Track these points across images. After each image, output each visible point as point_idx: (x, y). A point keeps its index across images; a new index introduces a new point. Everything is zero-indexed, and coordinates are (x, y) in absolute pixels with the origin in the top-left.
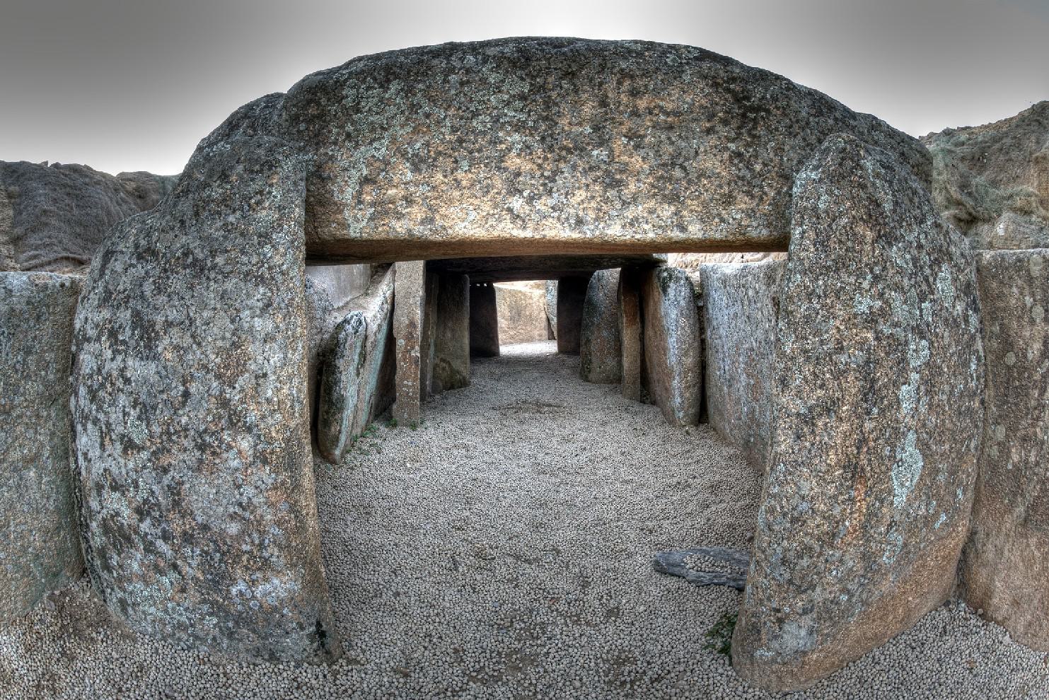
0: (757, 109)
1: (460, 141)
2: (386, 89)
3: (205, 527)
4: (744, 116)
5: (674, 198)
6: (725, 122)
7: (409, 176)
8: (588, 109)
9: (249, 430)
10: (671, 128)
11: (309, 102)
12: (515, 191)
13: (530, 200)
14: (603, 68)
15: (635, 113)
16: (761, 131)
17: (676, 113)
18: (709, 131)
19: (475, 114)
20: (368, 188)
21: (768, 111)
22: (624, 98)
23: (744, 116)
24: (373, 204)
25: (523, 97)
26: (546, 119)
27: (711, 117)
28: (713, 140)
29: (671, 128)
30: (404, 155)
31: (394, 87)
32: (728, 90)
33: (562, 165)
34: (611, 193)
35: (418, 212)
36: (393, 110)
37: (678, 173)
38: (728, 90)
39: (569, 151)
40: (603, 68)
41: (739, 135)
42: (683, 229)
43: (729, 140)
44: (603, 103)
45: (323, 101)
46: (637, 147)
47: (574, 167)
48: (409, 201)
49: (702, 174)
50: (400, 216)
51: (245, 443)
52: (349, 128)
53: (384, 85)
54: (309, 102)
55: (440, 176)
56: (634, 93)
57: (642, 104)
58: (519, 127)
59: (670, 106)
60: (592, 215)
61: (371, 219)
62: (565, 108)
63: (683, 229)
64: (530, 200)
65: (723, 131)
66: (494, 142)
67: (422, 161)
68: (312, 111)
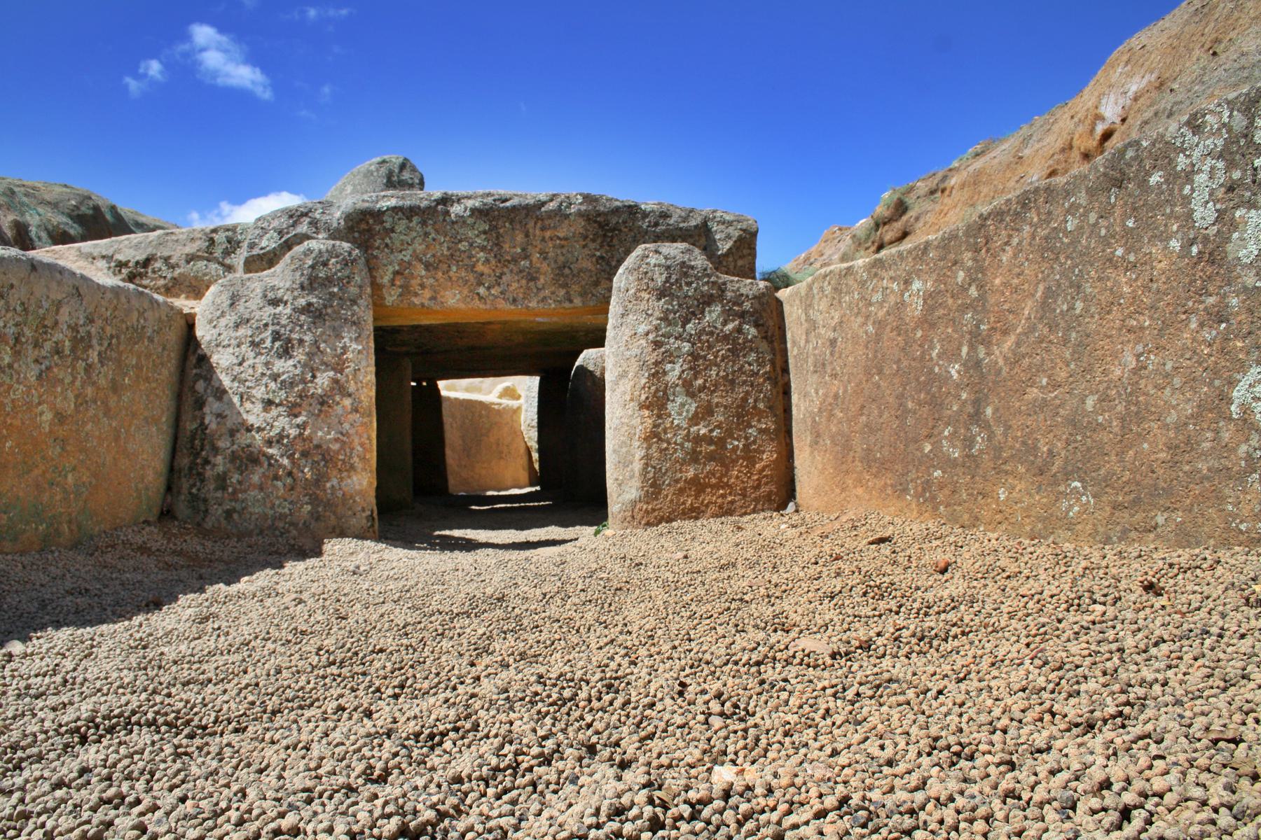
0: (613, 230)
1: (452, 255)
2: (411, 221)
3: (318, 447)
4: (605, 235)
5: (565, 286)
6: (593, 241)
7: (423, 273)
8: (520, 238)
9: (350, 395)
10: (563, 247)
11: (361, 220)
12: (480, 284)
13: (489, 288)
14: (527, 215)
15: (543, 240)
16: (615, 242)
17: (566, 239)
18: (584, 247)
19: (460, 241)
20: (398, 277)
21: (620, 231)
22: (538, 232)
23: (605, 235)
24: (401, 287)
25: (485, 232)
26: (497, 245)
27: (586, 238)
28: (586, 251)
29: (563, 247)
30: (421, 260)
31: (416, 219)
32: (596, 222)
33: (505, 270)
34: (532, 284)
35: (427, 294)
36: (414, 234)
37: (567, 271)
38: (596, 222)
39: (509, 262)
40: (527, 215)
41: (602, 246)
42: (571, 301)
43: (596, 250)
44: (527, 236)
45: (371, 221)
46: (545, 258)
47: (511, 271)
48: (422, 286)
49: (581, 270)
50: (416, 295)
51: (347, 402)
52: (387, 240)
53: (409, 219)
54: (361, 220)
55: (440, 274)
56: (543, 229)
57: (548, 234)
58: (483, 249)
59: (561, 235)
60: (521, 296)
61: (401, 295)
62: (507, 238)
63: (571, 301)
64: (489, 288)
65: (592, 246)
66: (470, 257)
67: (431, 265)
68: (363, 226)
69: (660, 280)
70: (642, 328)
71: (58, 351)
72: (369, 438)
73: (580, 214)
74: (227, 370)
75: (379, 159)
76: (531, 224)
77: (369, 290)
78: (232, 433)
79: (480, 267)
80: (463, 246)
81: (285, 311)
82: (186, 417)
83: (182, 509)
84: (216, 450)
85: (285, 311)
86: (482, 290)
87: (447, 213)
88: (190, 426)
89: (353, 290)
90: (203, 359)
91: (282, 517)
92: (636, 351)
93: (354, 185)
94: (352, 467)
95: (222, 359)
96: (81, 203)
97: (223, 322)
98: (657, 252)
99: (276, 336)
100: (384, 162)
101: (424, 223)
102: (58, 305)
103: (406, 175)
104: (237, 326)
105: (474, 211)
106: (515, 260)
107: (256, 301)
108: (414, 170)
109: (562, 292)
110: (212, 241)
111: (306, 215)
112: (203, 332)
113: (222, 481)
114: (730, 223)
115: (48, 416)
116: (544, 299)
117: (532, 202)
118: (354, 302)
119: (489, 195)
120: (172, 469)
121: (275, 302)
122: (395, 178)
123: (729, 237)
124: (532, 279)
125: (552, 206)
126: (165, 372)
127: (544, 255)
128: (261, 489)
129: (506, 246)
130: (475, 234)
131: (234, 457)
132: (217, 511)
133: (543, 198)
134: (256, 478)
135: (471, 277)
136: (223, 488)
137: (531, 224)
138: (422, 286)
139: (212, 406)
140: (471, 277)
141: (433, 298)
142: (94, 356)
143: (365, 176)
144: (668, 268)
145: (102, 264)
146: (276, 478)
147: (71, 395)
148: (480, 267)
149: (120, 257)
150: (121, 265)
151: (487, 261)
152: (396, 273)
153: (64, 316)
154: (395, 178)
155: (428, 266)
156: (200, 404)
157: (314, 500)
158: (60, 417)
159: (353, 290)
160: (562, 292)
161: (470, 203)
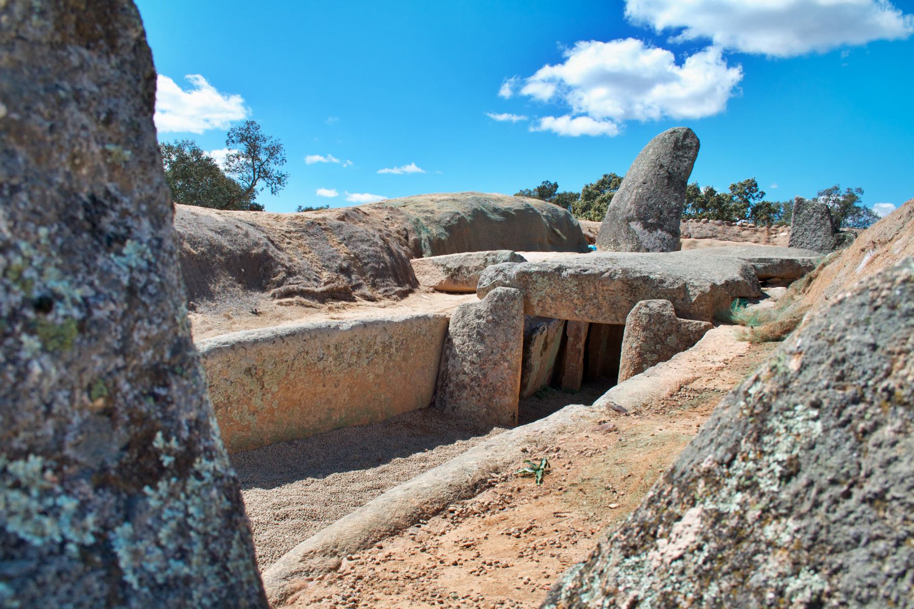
5: (614, 313)
8: (592, 289)
35: (553, 311)
51: (506, 364)
56: (603, 286)
57: (605, 288)
58: (576, 293)
69: (645, 321)
70: (634, 345)
71: (376, 352)
72: (515, 381)
73: (619, 279)
74: (458, 346)
75: (671, 130)
76: (597, 283)
77: (522, 312)
78: (457, 374)
79: (575, 301)
80: (567, 291)
81: (483, 321)
82: (442, 364)
83: (437, 404)
84: (451, 381)
85: (483, 321)
86: (577, 312)
87: (560, 275)
88: (443, 369)
89: (514, 312)
90: (450, 340)
91: (474, 412)
92: (630, 356)
93: (654, 149)
94: (506, 394)
95: (457, 341)
96: (452, 218)
97: (458, 324)
98: (646, 306)
99: (478, 333)
100: (674, 132)
101: (549, 279)
102: (376, 337)
103: (688, 141)
104: (463, 327)
105: (571, 275)
106: (591, 299)
107: (472, 316)
108: (694, 136)
109: (614, 316)
110: (486, 260)
111: (501, 271)
112: (451, 328)
113: (452, 393)
114: (696, 287)
115: (372, 376)
116: (605, 318)
117: (597, 272)
118: (514, 317)
119: (579, 267)
120: (436, 386)
121: (479, 317)
122: (680, 144)
123: (695, 295)
124: (599, 308)
125: (607, 274)
126: (433, 346)
127: (604, 298)
128: (466, 399)
129: (587, 292)
130: (572, 285)
131: (457, 385)
132: (449, 407)
133: (603, 270)
134: (465, 395)
135: (572, 305)
136: (452, 397)
137: (597, 283)
138: (551, 308)
139: (451, 361)
140: (572, 305)
141: (556, 313)
142: (393, 350)
143: (661, 142)
144: (650, 315)
145: (441, 268)
146: (473, 396)
147: (382, 367)
148: (575, 301)
149: (448, 266)
150: (449, 270)
151: (578, 298)
152: (539, 301)
153: (379, 339)
154: (680, 144)
155: (552, 299)
156: (447, 360)
157: (488, 407)
158: (377, 376)
159: (514, 312)
160: (614, 316)
161: (570, 271)
